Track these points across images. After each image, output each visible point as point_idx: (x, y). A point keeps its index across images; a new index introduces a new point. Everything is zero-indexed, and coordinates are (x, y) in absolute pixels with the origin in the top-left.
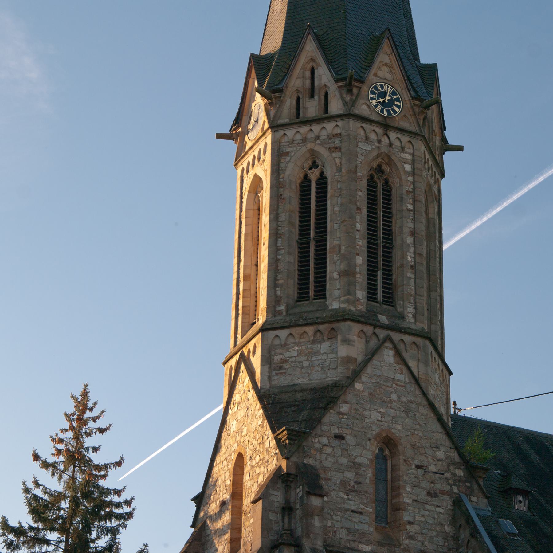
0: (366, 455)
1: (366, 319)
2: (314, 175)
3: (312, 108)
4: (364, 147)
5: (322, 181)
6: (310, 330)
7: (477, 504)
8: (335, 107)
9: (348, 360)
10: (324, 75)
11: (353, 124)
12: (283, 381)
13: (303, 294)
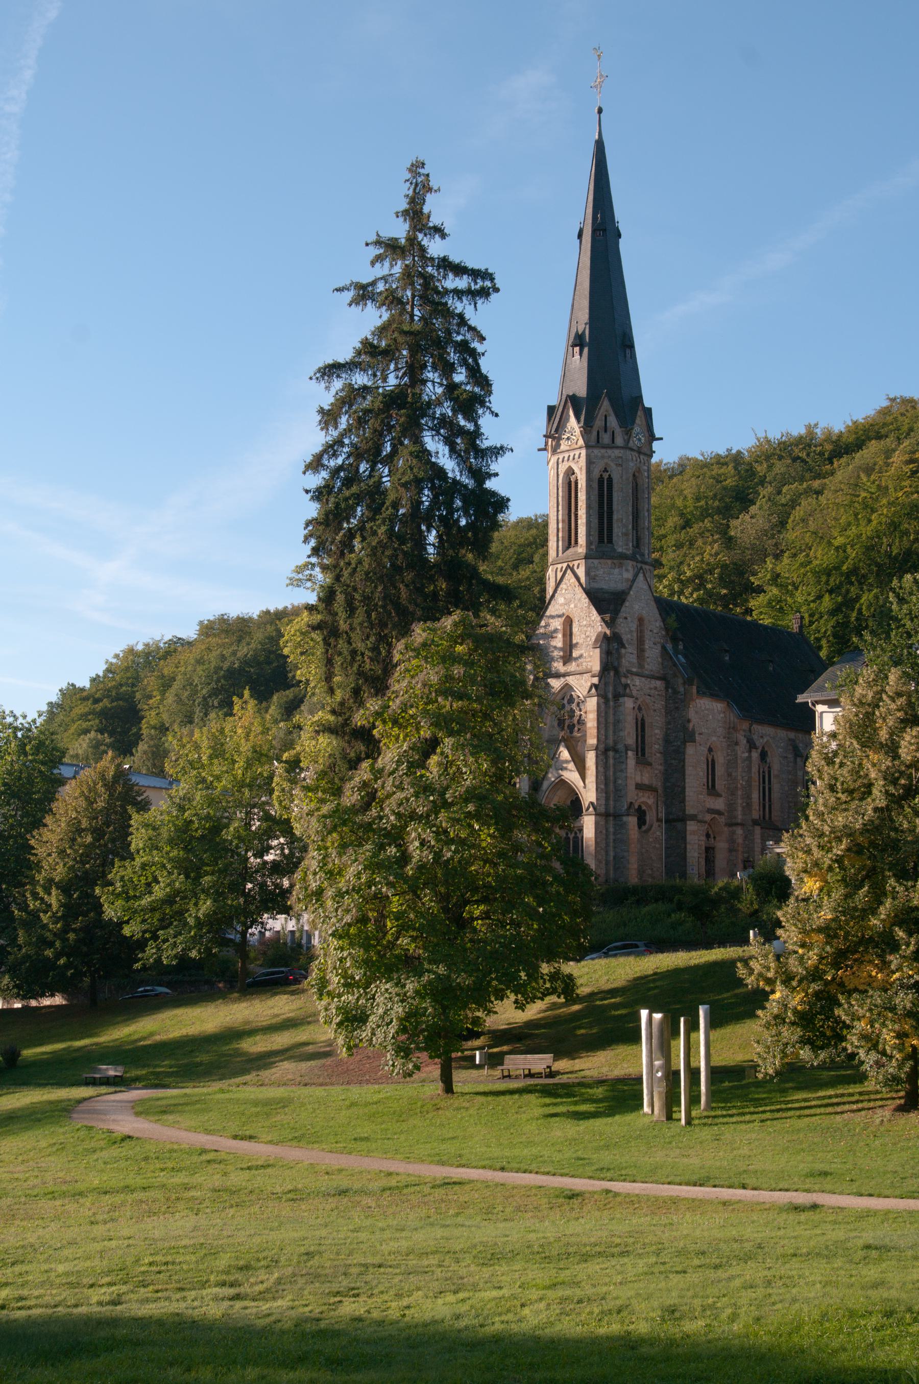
0: (634, 626)
1: (633, 558)
2: (606, 476)
3: (606, 438)
4: (631, 464)
5: (610, 479)
6: (609, 562)
7: (669, 646)
8: (619, 441)
9: (627, 580)
10: (613, 422)
11: (628, 452)
12: (596, 585)
13: (601, 540)
